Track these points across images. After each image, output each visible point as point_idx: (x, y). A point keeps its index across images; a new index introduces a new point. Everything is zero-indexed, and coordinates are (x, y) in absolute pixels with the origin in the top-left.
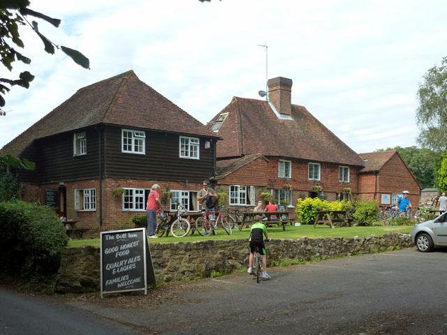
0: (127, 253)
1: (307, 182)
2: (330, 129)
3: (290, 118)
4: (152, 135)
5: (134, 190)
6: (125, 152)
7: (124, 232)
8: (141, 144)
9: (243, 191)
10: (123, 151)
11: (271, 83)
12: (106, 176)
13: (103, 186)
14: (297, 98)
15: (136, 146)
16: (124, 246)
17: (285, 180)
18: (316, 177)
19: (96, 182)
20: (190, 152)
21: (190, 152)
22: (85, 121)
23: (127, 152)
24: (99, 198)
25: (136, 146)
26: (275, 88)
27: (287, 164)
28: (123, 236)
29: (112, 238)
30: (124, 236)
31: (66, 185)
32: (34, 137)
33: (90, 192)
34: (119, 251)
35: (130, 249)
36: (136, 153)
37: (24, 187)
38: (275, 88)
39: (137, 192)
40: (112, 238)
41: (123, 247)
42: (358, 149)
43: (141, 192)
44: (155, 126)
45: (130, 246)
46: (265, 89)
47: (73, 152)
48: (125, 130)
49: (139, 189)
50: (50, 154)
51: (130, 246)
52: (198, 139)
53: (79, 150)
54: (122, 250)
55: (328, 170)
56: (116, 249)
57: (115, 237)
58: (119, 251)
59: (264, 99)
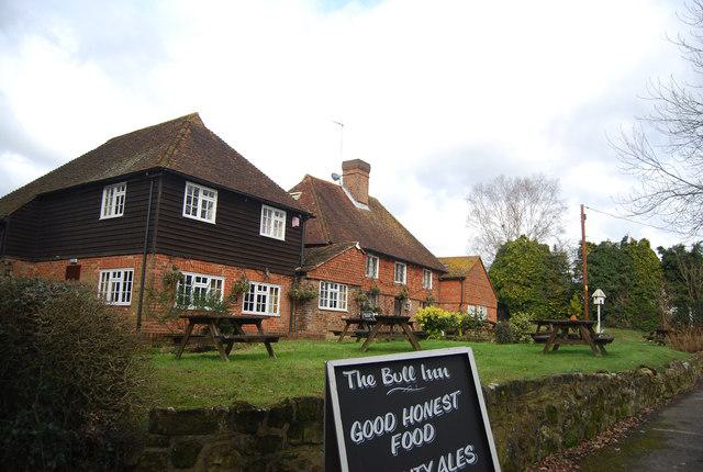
0: (427, 435)
1: (393, 285)
2: (405, 226)
3: (366, 208)
4: (227, 198)
5: (194, 276)
6: (187, 216)
7: (407, 362)
8: (211, 206)
9: (333, 290)
10: (184, 215)
11: (347, 166)
12: (156, 250)
13: (149, 265)
14: (374, 191)
15: (203, 208)
16: (414, 411)
17: (372, 279)
18: (401, 280)
19: (139, 259)
20: (273, 227)
21: (273, 227)
22: (129, 166)
23: (190, 216)
24: (139, 286)
25: (203, 208)
26: (351, 172)
27: (374, 260)
28: (403, 376)
29: (366, 381)
30: (407, 374)
31: (81, 262)
32: (37, 192)
33: (123, 275)
34: (400, 429)
35: (433, 420)
36: (203, 220)
37: (10, 264)
38: (351, 172)
39: (198, 280)
40: (366, 381)
41: (411, 415)
42: (438, 252)
43: (205, 281)
44: (233, 186)
45: (431, 409)
46: (340, 172)
47: (99, 213)
48: (191, 184)
49: (202, 276)
50: (56, 211)
51: (431, 409)
52: (285, 213)
53: (111, 206)
54: (411, 428)
55: (413, 272)
56: (383, 424)
57: (379, 378)
58: (400, 429)
59: (337, 183)
